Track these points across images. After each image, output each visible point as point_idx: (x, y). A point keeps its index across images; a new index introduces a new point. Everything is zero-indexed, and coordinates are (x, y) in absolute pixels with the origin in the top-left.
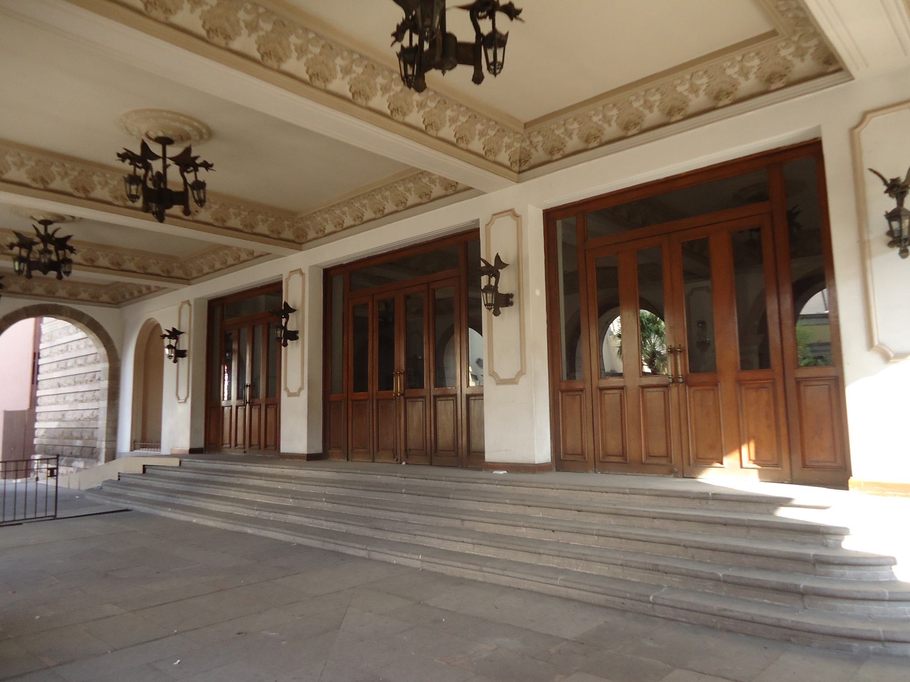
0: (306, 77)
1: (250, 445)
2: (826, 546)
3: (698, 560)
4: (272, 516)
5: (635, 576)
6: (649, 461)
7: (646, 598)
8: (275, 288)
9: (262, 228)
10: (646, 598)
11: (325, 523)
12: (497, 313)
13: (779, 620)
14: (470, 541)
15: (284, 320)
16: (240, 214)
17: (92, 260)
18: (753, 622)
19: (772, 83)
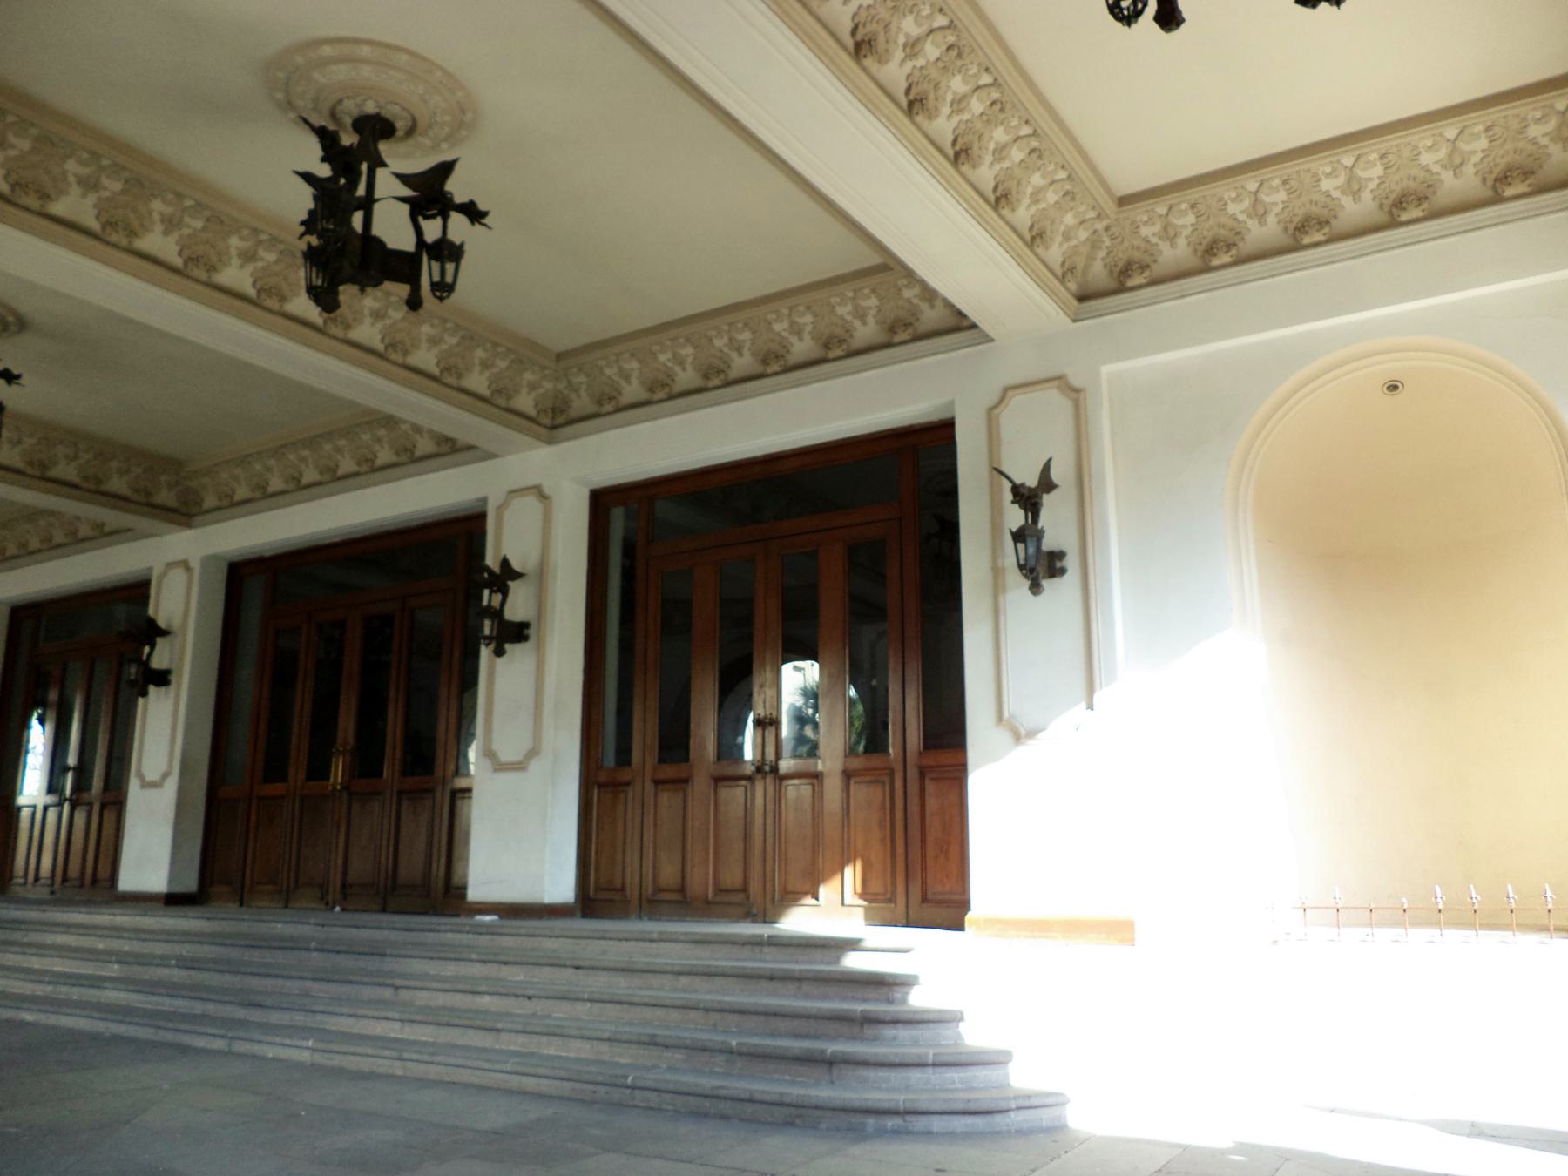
0: (178, 262)
1: (65, 879)
2: (890, 1001)
3: (721, 1029)
4: (75, 993)
5: (625, 1056)
6: (718, 899)
7: (622, 1080)
8: (137, 591)
9: (118, 485)
10: (622, 1080)
11: (167, 1000)
12: (499, 652)
13: (782, 1095)
14: (397, 1016)
15: (147, 649)
18: (752, 1101)
19: (1215, 255)
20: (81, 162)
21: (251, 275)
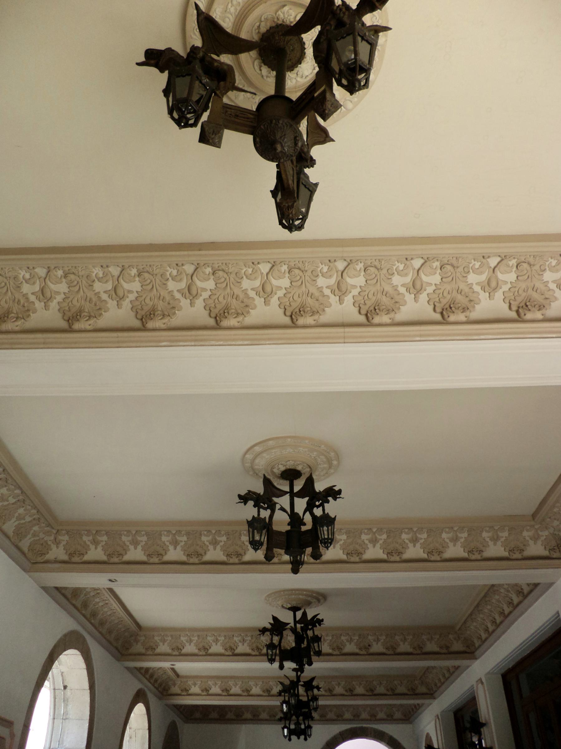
9: (431, 647)
16: (405, 639)
17: (207, 690)
20: (366, 534)
21: (461, 547)
